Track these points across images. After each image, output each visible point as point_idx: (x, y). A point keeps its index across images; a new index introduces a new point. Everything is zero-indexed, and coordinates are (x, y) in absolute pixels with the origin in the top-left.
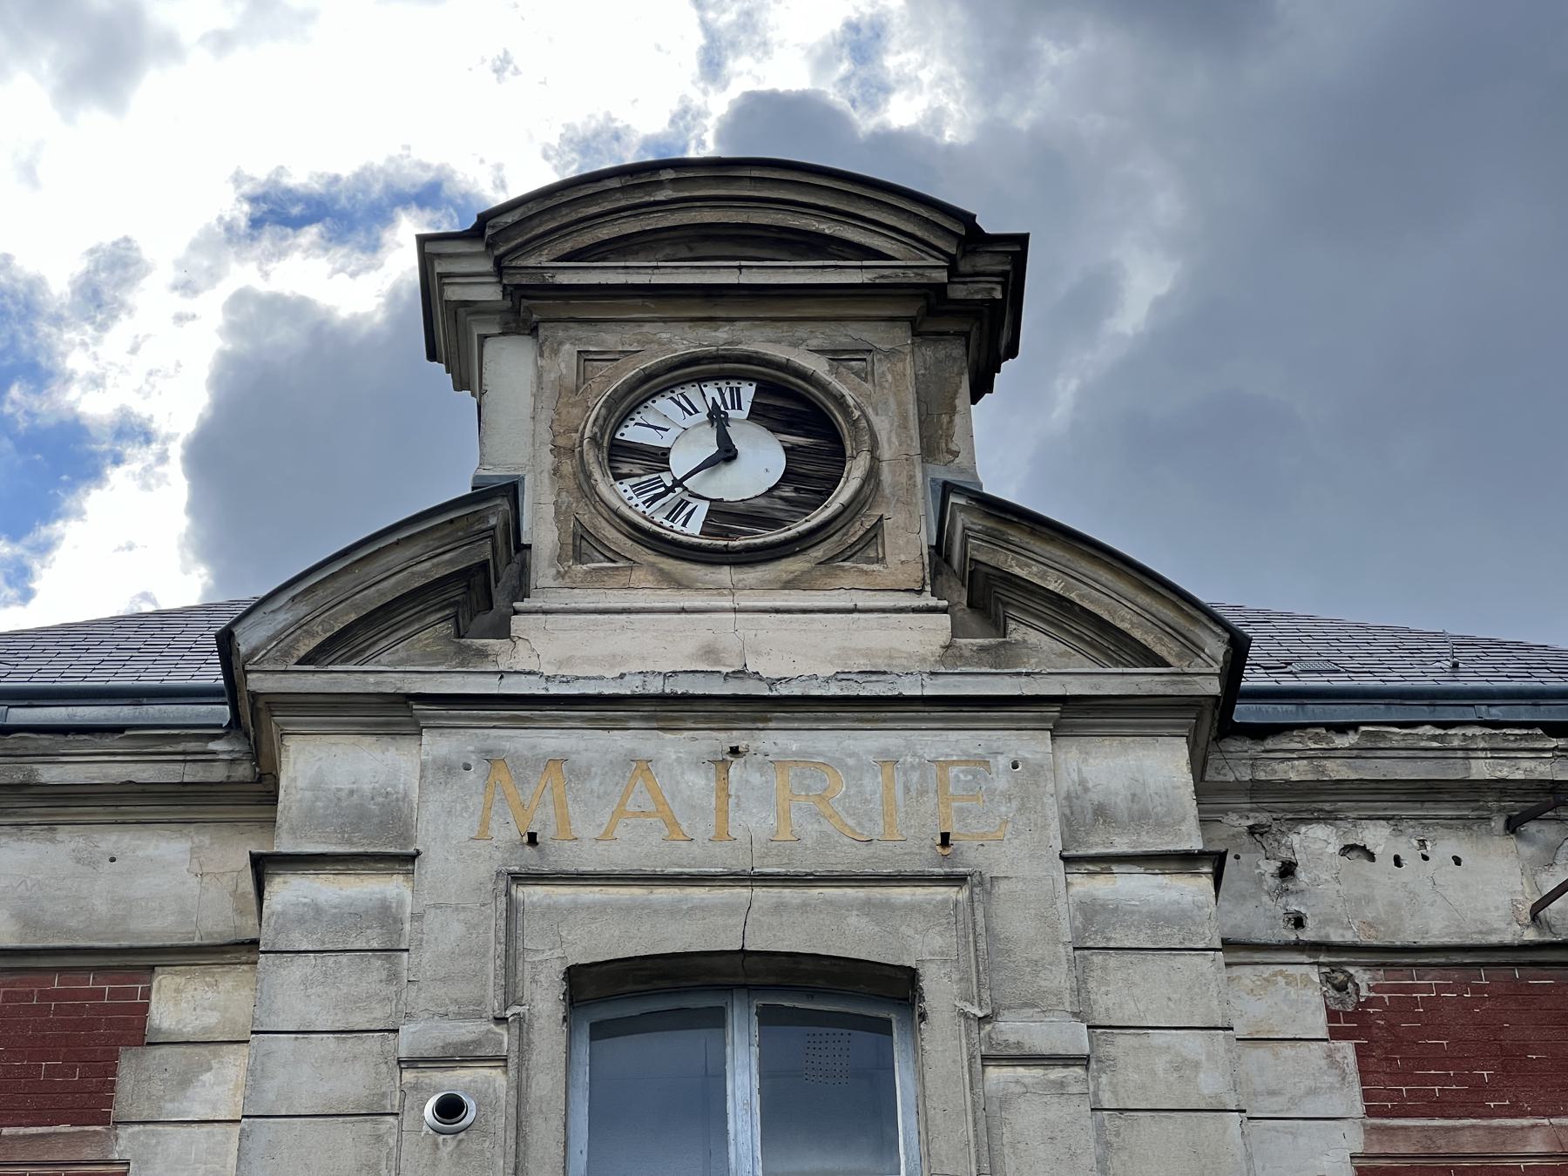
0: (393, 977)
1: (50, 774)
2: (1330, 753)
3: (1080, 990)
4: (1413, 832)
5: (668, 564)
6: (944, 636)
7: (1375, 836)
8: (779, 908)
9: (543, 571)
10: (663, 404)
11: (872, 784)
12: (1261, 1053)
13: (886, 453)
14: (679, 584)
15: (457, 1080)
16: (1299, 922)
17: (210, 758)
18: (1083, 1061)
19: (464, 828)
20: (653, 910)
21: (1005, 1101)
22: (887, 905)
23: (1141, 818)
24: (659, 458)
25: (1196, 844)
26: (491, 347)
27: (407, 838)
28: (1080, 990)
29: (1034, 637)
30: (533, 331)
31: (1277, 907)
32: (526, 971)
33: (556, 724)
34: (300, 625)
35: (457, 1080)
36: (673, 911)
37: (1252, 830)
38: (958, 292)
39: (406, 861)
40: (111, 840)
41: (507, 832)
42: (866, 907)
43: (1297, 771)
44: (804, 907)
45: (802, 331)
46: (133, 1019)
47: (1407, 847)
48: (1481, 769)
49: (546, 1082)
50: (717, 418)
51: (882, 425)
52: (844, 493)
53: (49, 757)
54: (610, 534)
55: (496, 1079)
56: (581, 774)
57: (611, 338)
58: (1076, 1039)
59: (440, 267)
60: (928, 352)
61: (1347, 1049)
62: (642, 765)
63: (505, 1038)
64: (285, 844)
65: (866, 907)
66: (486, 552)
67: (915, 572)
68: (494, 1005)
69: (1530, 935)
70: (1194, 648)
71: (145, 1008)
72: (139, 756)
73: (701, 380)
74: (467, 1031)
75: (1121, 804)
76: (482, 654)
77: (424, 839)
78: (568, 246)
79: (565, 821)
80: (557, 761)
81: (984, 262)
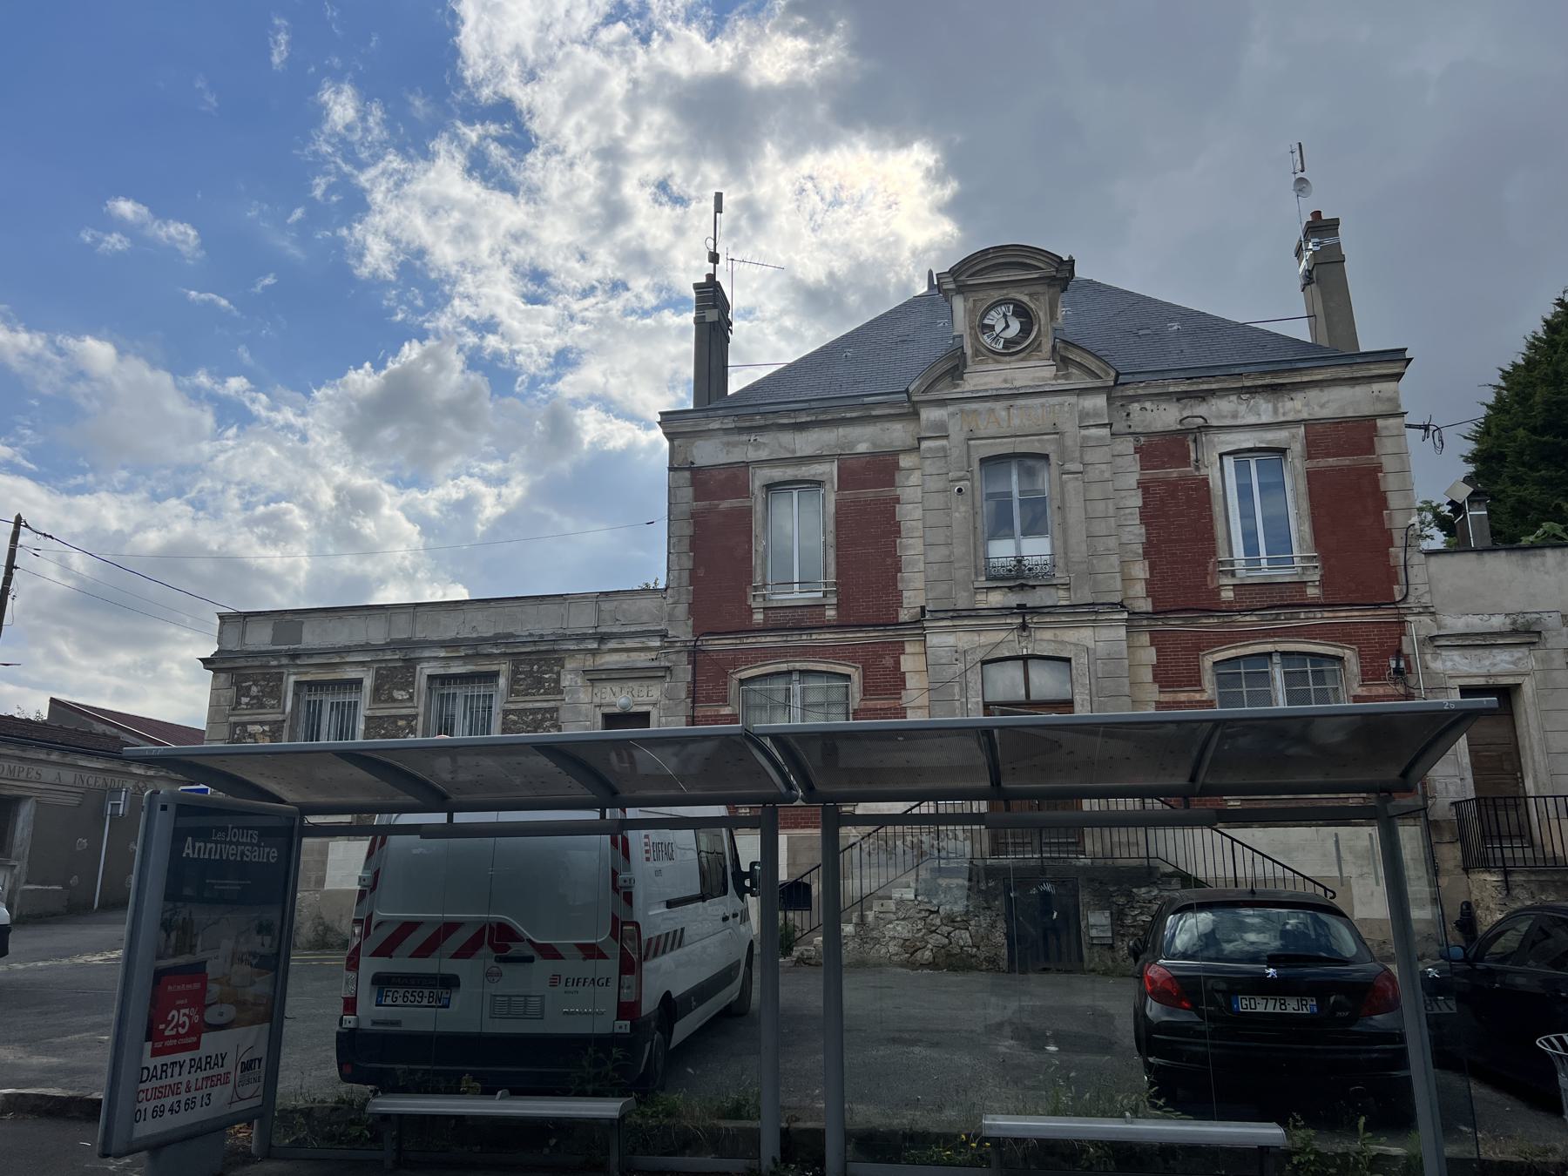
0: (946, 462)
1: (874, 413)
2: (1138, 388)
3: (1081, 457)
4: (1156, 402)
5: (996, 357)
6: (1054, 373)
7: (1148, 405)
8: (1021, 442)
9: (969, 362)
10: (993, 313)
11: (1040, 411)
13: (1042, 323)
14: (998, 362)
16: (1130, 427)
17: (904, 407)
18: (1081, 473)
19: (958, 428)
20: (996, 444)
22: (1042, 440)
24: (992, 327)
25: (1107, 422)
28: (1081, 457)
29: (1074, 371)
34: (921, 384)
36: (1001, 444)
37: (1122, 405)
38: (1059, 275)
39: (947, 437)
40: (887, 425)
41: (966, 429)
42: (1039, 440)
43: (1131, 393)
44: (1026, 442)
45: (1023, 289)
46: (1186, 1062)
47: (1154, 407)
48: (1171, 389)
49: (977, 484)
50: (1005, 316)
56: (980, 413)
57: (980, 295)
58: (1076, 467)
59: (941, 281)
60: (1051, 290)
61: (1138, 456)
62: (993, 410)
63: (969, 475)
64: (923, 434)
69: (1179, 427)
72: (891, 407)
73: (1001, 305)
74: (962, 473)
76: (958, 385)
77: (951, 431)
79: (977, 425)
80: (975, 411)
81: (1064, 267)
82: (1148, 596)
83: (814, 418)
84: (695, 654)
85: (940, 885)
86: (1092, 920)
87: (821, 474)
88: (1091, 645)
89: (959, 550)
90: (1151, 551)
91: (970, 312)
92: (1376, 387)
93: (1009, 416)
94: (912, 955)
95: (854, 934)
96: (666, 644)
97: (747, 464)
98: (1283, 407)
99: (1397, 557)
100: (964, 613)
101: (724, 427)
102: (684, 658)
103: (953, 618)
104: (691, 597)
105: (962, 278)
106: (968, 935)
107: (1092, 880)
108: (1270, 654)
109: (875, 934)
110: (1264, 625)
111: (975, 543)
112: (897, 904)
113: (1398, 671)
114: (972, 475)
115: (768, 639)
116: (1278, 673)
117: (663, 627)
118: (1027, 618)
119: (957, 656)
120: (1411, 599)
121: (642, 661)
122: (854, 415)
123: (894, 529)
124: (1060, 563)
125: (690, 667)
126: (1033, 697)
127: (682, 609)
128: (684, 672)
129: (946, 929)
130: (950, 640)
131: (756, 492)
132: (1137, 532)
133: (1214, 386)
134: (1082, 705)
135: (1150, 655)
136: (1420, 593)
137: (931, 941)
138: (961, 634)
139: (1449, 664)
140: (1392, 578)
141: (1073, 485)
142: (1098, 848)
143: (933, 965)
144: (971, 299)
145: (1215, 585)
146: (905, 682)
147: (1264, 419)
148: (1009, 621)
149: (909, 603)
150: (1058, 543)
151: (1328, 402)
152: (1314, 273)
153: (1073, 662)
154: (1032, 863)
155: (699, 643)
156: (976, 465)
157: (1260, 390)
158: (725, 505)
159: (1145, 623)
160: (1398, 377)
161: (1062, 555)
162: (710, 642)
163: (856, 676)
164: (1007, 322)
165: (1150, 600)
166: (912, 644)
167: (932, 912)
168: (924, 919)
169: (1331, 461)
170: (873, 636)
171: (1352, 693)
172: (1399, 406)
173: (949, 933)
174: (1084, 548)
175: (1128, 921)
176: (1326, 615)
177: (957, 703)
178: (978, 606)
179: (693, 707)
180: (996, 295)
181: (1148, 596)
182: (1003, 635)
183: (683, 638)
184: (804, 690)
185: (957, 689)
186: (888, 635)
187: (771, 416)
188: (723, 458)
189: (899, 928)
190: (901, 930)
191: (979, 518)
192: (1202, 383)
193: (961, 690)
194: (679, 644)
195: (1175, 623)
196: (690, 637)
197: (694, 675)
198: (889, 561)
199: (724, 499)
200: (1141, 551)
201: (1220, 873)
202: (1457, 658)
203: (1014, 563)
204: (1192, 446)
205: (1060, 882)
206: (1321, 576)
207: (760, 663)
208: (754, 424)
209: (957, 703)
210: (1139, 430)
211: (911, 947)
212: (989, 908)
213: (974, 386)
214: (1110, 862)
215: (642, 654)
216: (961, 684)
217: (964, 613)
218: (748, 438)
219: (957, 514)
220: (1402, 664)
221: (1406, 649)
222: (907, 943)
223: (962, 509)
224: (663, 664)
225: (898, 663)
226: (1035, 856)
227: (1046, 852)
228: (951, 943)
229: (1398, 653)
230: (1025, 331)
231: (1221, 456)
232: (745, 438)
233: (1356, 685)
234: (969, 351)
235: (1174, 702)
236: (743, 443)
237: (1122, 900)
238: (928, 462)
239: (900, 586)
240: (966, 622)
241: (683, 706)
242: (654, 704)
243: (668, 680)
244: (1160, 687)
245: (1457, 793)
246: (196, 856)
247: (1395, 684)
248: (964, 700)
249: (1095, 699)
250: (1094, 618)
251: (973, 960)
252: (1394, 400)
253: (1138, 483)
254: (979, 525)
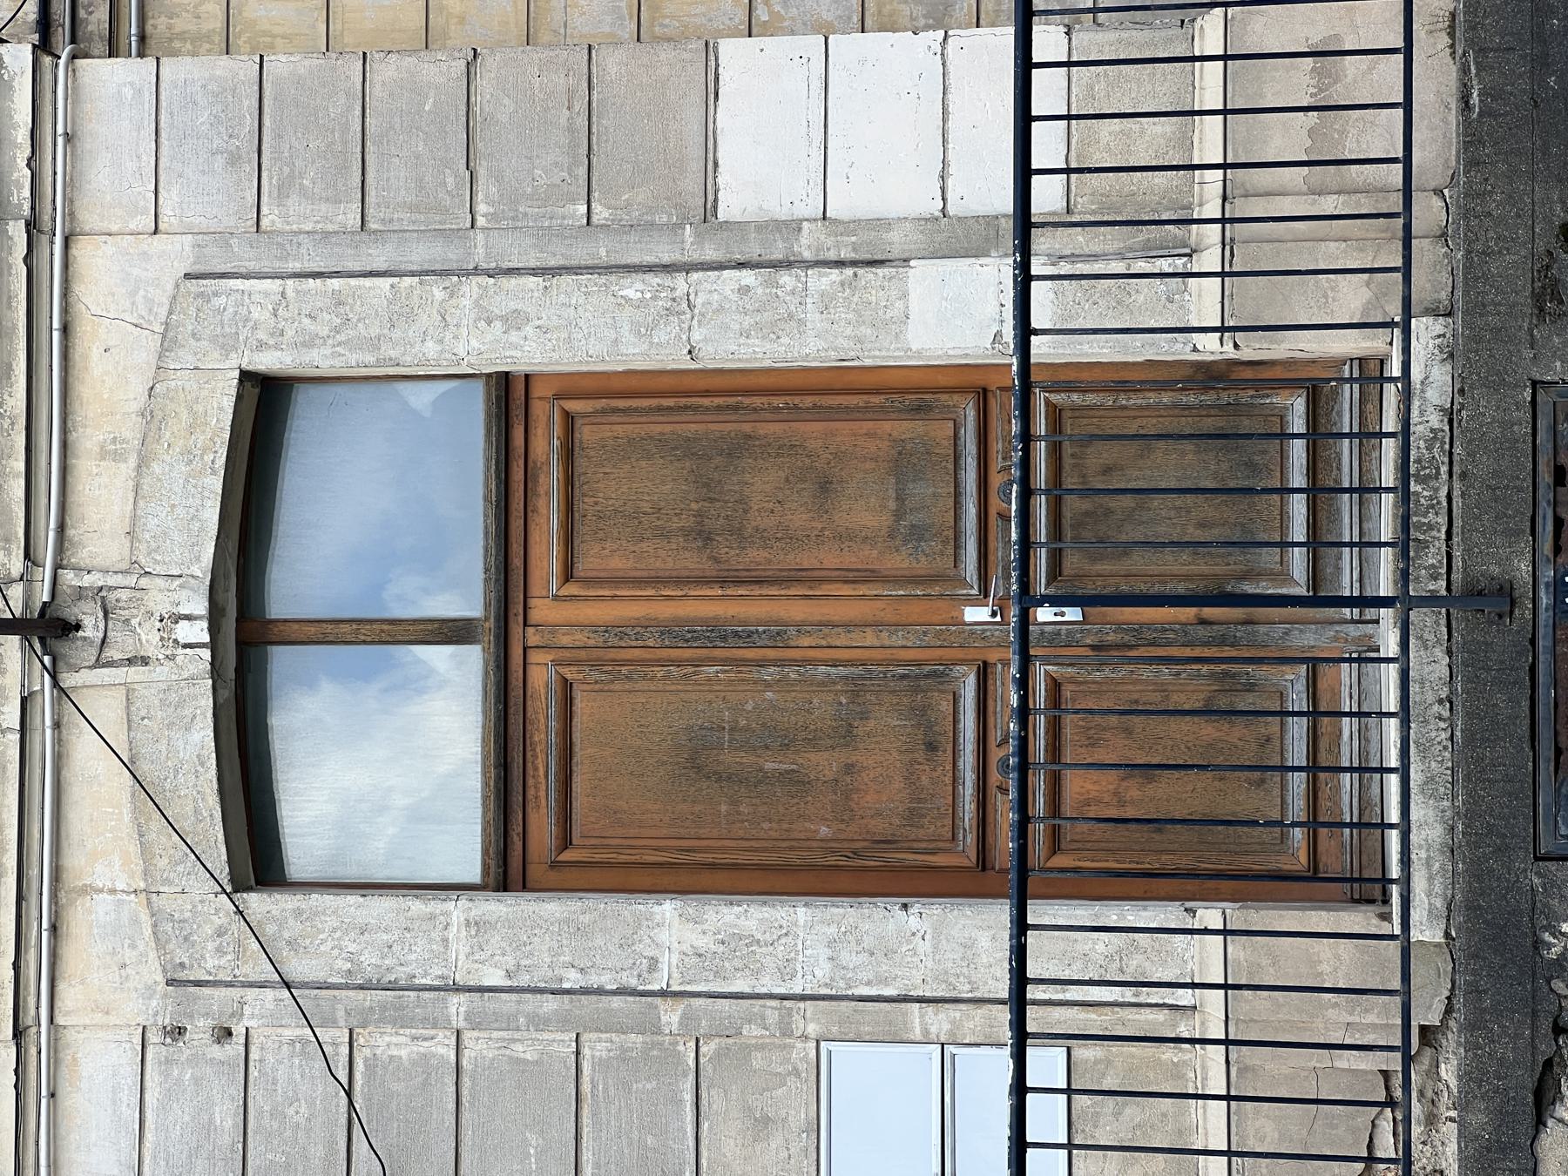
36: (829, 590)
88: (176, 253)
119: (199, 1030)
134: (514, 320)
138: (69, 995)
142: (1351, 299)
153: (267, 362)
154: (1431, 666)
177: (478, 1047)
182: (87, 756)
193: (401, 1020)
214: (1429, 212)
216: (365, 1018)
226: (1391, 647)
238: (96, 870)
246: (1311, 594)
248: (457, 1005)
249: (480, 251)
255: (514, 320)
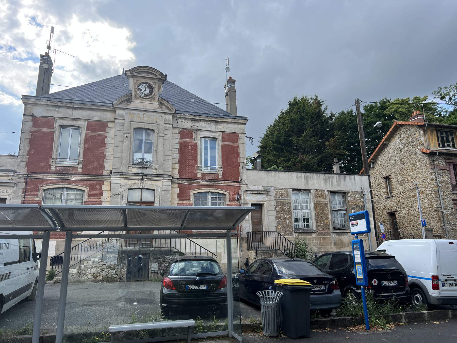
1: (101, 108)
2: (181, 115)
7: (183, 120)
9: (133, 98)
10: (141, 85)
11: (153, 117)
12: (174, 134)
13: (156, 91)
14: (142, 100)
15: (127, 135)
17: (111, 108)
18: (163, 137)
19: (128, 118)
21: (159, 139)
22: (153, 125)
23: (169, 121)
24: (141, 90)
26: (130, 78)
27: (124, 118)
29: (164, 107)
30: (133, 77)
31: (177, 125)
32: (131, 128)
33: (134, 111)
34: (117, 102)
35: (127, 135)
38: (162, 79)
40: (105, 113)
41: (130, 118)
42: (152, 125)
43: (179, 116)
44: (148, 125)
45: (151, 80)
48: (190, 117)
49: (132, 135)
50: (145, 87)
51: (156, 89)
52: (153, 95)
53: (101, 107)
54: (137, 95)
55: (129, 135)
57: (138, 79)
60: (159, 83)
61: (179, 134)
62: (139, 114)
63: (130, 132)
65: (152, 125)
66: (129, 98)
67: (157, 101)
68: (129, 130)
69: (191, 128)
70: (173, 110)
71: (107, 125)
73: (144, 83)
74: (128, 131)
75: (168, 120)
76: (129, 105)
78: (135, 72)
79: (134, 118)
80: (133, 113)
81: (164, 77)
82: (178, 174)
83: (80, 106)
84: (26, 179)
85: (107, 256)
86: (152, 266)
87: (81, 125)
88: (161, 186)
89: (125, 154)
90: (180, 161)
91: (135, 84)
92: (240, 126)
93: (144, 117)
94: (96, 278)
95: (76, 272)
96: (16, 175)
97: (54, 118)
98: (218, 127)
99: (240, 170)
100: (124, 174)
101: (46, 104)
102: (23, 180)
103: (120, 175)
104: (28, 159)
105: (133, 73)
106: (114, 271)
107: (154, 254)
108: (208, 192)
109: (84, 272)
110: (207, 184)
111: (130, 153)
112: (92, 262)
113: (238, 199)
114: (131, 133)
115: (56, 176)
116: (209, 197)
117: (15, 169)
118: (143, 177)
120: (242, 181)
121: (5, 180)
122: (94, 108)
123: (105, 146)
124: (155, 162)
125: (25, 183)
126: (143, 200)
127: (23, 164)
128: (22, 185)
129: (107, 270)
130: (119, 181)
131: (57, 127)
132: (177, 155)
133: (201, 119)
134: (157, 203)
135: (177, 190)
136: (244, 180)
137: (102, 273)
139: (249, 198)
140: (239, 175)
141: (161, 140)
143: (102, 281)
144: (135, 80)
145: (196, 172)
146: (103, 193)
147: (213, 130)
148: (138, 177)
149: (107, 169)
150: (155, 156)
151: (228, 127)
152: (228, 93)
154: (137, 249)
155: (29, 176)
156: (132, 130)
157: (212, 121)
158: (44, 130)
159: (177, 181)
160: (245, 124)
161: (156, 160)
162: (33, 176)
163: (86, 190)
164: (145, 89)
165: (179, 175)
166: (107, 182)
167: (104, 265)
168: (101, 267)
169: (228, 143)
170: (94, 178)
171: (227, 204)
172: (244, 131)
173: (108, 271)
174: (162, 158)
175: (163, 266)
176: (223, 183)
177: (119, 201)
178: (129, 172)
179: (24, 197)
180: (143, 80)
181: (178, 174)
183: (23, 173)
184: (67, 194)
185: (119, 197)
186: (99, 178)
187: (64, 103)
188: (45, 114)
189: (92, 270)
190: (93, 270)
191: (132, 145)
192: (198, 117)
193: (121, 197)
194: (21, 175)
195: (185, 182)
196: (26, 173)
197: (26, 186)
198: (101, 155)
199: (44, 128)
200: (178, 161)
201: (189, 251)
202: (251, 196)
203: (142, 160)
204: (194, 134)
205: (144, 254)
206: (223, 173)
207: (52, 184)
208: (58, 105)
209: (119, 201)
210: (180, 127)
211: (95, 276)
212: (122, 263)
213: (134, 106)
214: (160, 249)
215: (6, 178)
217: (124, 174)
218: (55, 109)
219: (125, 144)
220: (239, 197)
221: (240, 193)
222: (94, 275)
223: (127, 142)
224: (13, 182)
225: (101, 187)
227: (141, 246)
228: (109, 274)
229: (238, 194)
230: (151, 92)
231: (201, 138)
232: (54, 109)
233: (228, 202)
234: (133, 95)
235: (182, 204)
236: (53, 110)
237: (162, 260)
239: (104, 164)
240: (124, 177)
241: (20, 197)
242: (9, 195)
243: (15, 187)
244: (179, 199)
245: (248, 230)
247: (237, 202)
248: (121, 200)
250: (163, 178)
251: (115, 279)
252: (243, 130)
253: (179, 142)
254: (132, 147)
255: (157, 203)
